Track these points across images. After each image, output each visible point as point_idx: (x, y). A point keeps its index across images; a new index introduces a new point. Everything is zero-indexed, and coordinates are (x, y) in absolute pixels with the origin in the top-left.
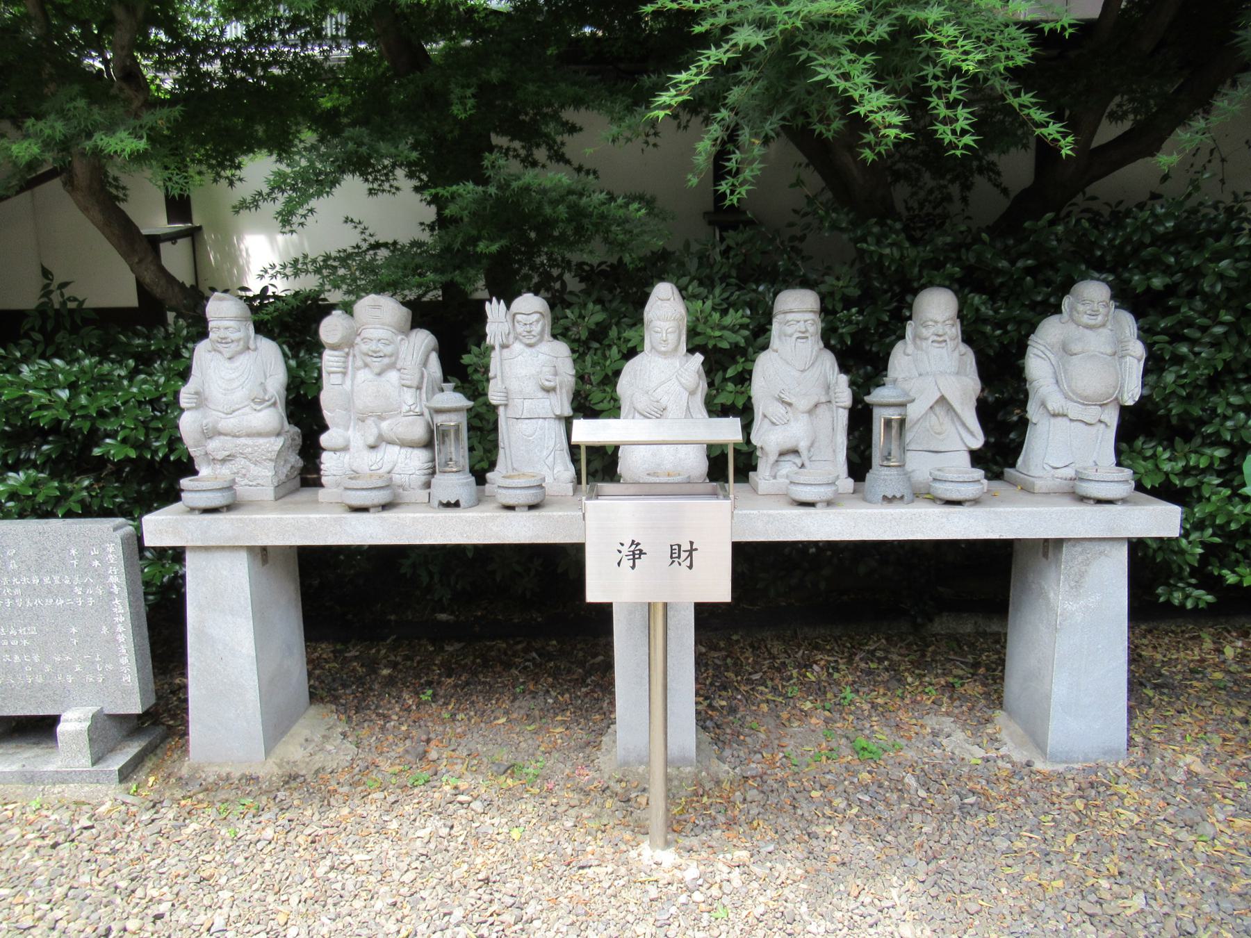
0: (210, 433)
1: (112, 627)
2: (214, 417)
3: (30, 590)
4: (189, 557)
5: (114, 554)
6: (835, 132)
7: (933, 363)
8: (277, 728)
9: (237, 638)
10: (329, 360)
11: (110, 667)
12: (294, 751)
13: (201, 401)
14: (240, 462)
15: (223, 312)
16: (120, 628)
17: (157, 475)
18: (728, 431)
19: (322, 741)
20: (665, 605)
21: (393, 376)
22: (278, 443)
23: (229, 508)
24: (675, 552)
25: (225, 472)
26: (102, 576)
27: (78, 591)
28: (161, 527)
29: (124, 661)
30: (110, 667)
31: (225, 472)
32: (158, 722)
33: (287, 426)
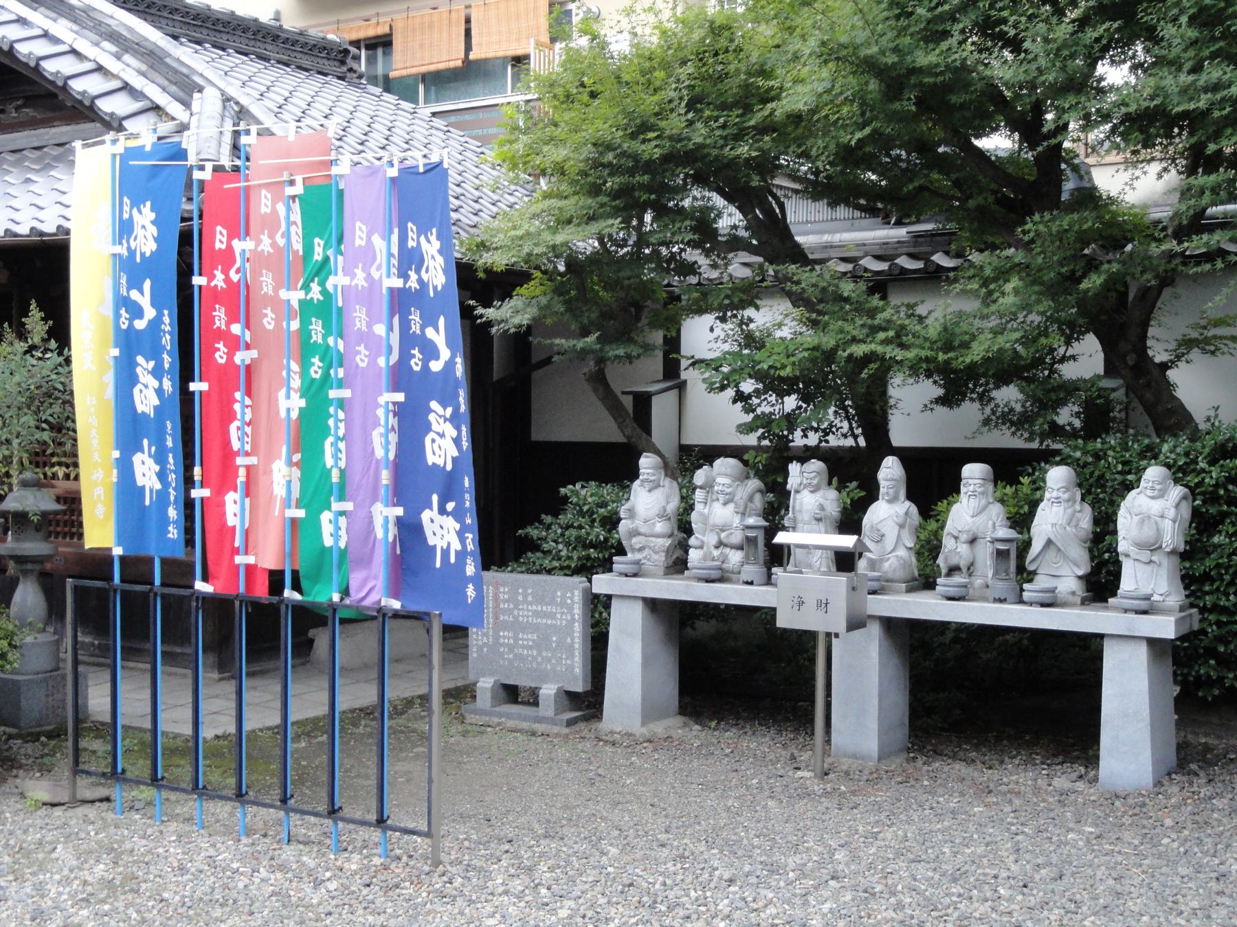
0: (635, 533)
1: (573, 639)
2: (638, 524)
3: (537, 614)
4: (615, 604)
5: (578, 596)
6: (526, 535)
7: (1059, 511)
8: (650, 713)
9: (636, 666)
10: (699, 495)
11: (569, 662)
12: (659, 728)
13: (632, 514)
14: (646, 552)
15: (647, 462)
16: (577, 640)
17: (601, 553)
18: (847, 541)
19: (673, 726)
20: (828, 635)
21: (731, 506)
22: (667, 542)
23: (635, 575)
24: (819, 603)
25: (638, 556)
26: (571, 609)
27: (558, 616)
28: (602, 583)
29: (577, 659)
30: (569, 662)
31: (638, 556)
32: (588, 702)
33: (676, 532)
